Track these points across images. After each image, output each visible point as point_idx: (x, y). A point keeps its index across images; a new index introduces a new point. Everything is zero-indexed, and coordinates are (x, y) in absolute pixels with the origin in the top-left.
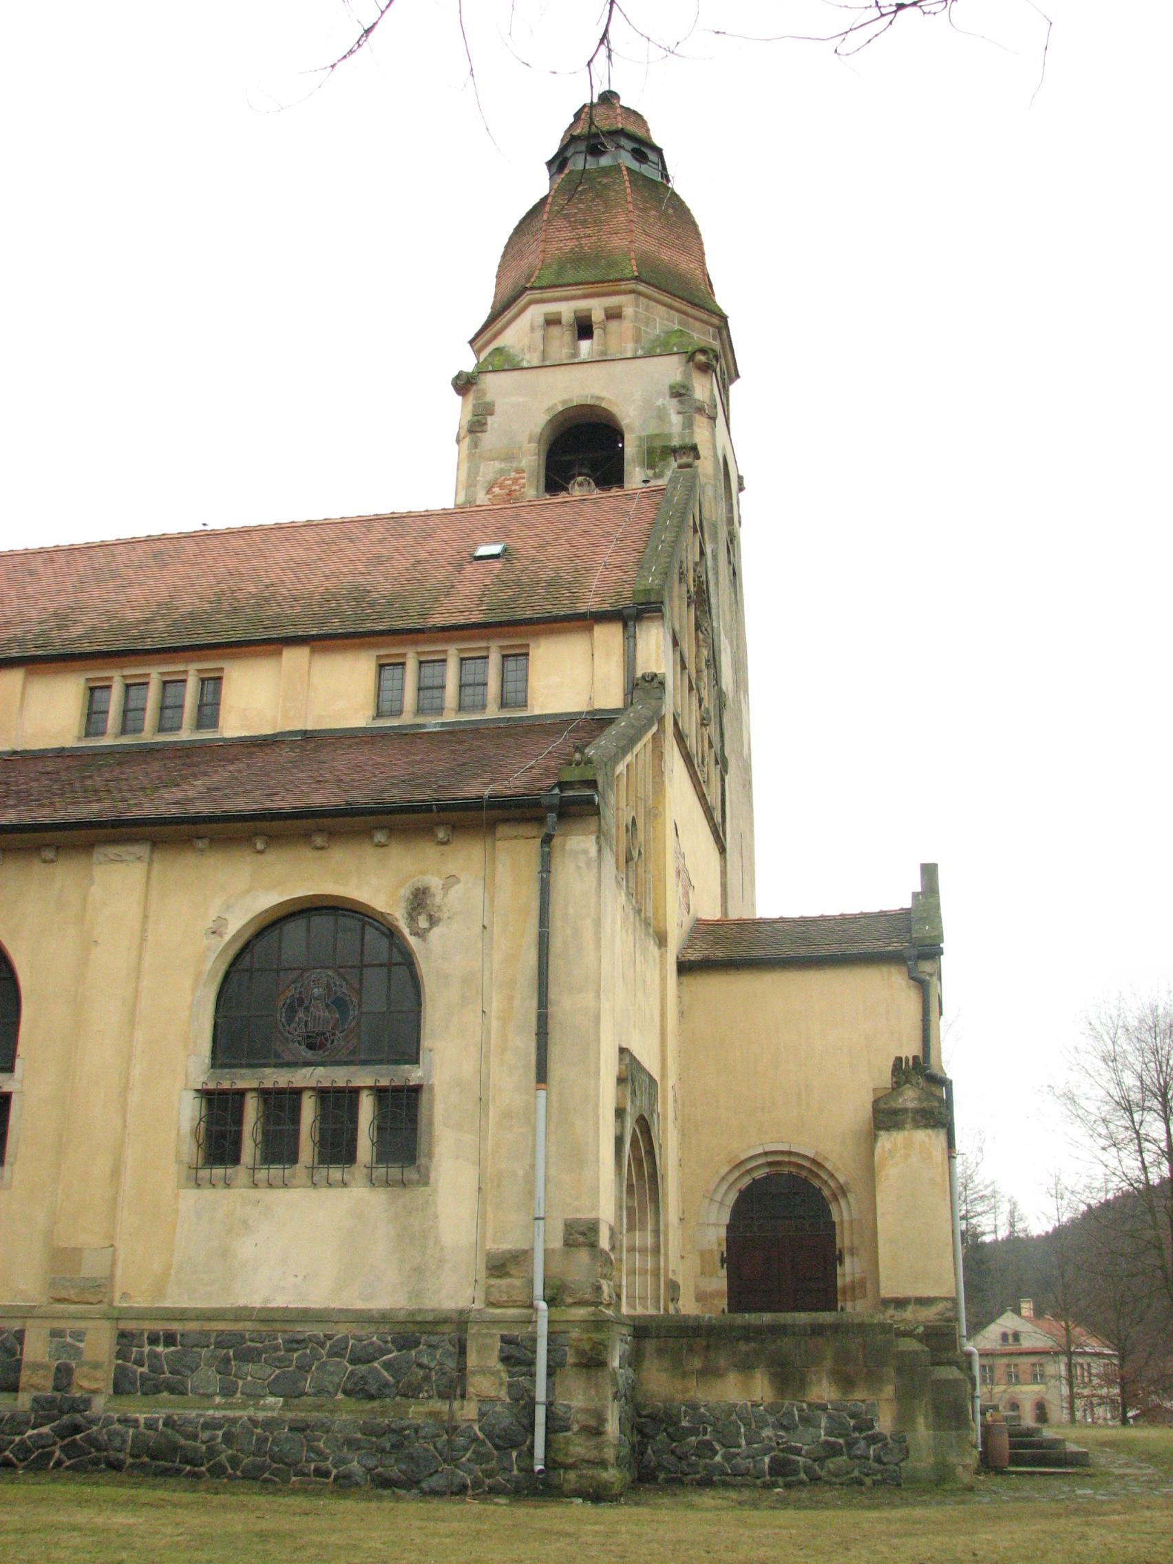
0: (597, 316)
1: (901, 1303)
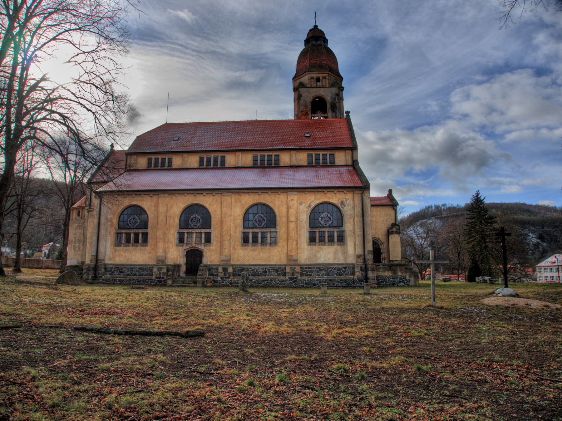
0: (321, 78)
1: (393, 261)
